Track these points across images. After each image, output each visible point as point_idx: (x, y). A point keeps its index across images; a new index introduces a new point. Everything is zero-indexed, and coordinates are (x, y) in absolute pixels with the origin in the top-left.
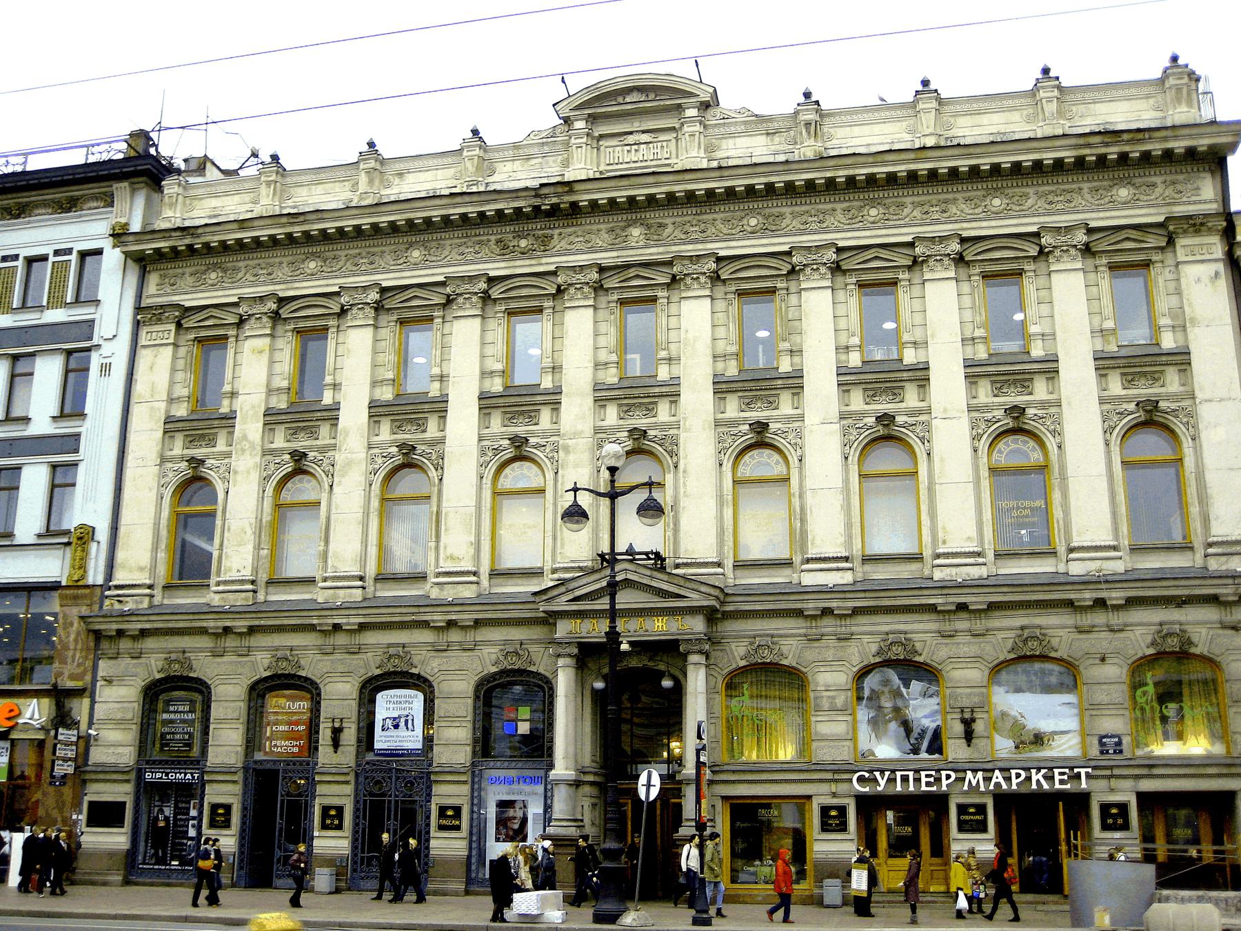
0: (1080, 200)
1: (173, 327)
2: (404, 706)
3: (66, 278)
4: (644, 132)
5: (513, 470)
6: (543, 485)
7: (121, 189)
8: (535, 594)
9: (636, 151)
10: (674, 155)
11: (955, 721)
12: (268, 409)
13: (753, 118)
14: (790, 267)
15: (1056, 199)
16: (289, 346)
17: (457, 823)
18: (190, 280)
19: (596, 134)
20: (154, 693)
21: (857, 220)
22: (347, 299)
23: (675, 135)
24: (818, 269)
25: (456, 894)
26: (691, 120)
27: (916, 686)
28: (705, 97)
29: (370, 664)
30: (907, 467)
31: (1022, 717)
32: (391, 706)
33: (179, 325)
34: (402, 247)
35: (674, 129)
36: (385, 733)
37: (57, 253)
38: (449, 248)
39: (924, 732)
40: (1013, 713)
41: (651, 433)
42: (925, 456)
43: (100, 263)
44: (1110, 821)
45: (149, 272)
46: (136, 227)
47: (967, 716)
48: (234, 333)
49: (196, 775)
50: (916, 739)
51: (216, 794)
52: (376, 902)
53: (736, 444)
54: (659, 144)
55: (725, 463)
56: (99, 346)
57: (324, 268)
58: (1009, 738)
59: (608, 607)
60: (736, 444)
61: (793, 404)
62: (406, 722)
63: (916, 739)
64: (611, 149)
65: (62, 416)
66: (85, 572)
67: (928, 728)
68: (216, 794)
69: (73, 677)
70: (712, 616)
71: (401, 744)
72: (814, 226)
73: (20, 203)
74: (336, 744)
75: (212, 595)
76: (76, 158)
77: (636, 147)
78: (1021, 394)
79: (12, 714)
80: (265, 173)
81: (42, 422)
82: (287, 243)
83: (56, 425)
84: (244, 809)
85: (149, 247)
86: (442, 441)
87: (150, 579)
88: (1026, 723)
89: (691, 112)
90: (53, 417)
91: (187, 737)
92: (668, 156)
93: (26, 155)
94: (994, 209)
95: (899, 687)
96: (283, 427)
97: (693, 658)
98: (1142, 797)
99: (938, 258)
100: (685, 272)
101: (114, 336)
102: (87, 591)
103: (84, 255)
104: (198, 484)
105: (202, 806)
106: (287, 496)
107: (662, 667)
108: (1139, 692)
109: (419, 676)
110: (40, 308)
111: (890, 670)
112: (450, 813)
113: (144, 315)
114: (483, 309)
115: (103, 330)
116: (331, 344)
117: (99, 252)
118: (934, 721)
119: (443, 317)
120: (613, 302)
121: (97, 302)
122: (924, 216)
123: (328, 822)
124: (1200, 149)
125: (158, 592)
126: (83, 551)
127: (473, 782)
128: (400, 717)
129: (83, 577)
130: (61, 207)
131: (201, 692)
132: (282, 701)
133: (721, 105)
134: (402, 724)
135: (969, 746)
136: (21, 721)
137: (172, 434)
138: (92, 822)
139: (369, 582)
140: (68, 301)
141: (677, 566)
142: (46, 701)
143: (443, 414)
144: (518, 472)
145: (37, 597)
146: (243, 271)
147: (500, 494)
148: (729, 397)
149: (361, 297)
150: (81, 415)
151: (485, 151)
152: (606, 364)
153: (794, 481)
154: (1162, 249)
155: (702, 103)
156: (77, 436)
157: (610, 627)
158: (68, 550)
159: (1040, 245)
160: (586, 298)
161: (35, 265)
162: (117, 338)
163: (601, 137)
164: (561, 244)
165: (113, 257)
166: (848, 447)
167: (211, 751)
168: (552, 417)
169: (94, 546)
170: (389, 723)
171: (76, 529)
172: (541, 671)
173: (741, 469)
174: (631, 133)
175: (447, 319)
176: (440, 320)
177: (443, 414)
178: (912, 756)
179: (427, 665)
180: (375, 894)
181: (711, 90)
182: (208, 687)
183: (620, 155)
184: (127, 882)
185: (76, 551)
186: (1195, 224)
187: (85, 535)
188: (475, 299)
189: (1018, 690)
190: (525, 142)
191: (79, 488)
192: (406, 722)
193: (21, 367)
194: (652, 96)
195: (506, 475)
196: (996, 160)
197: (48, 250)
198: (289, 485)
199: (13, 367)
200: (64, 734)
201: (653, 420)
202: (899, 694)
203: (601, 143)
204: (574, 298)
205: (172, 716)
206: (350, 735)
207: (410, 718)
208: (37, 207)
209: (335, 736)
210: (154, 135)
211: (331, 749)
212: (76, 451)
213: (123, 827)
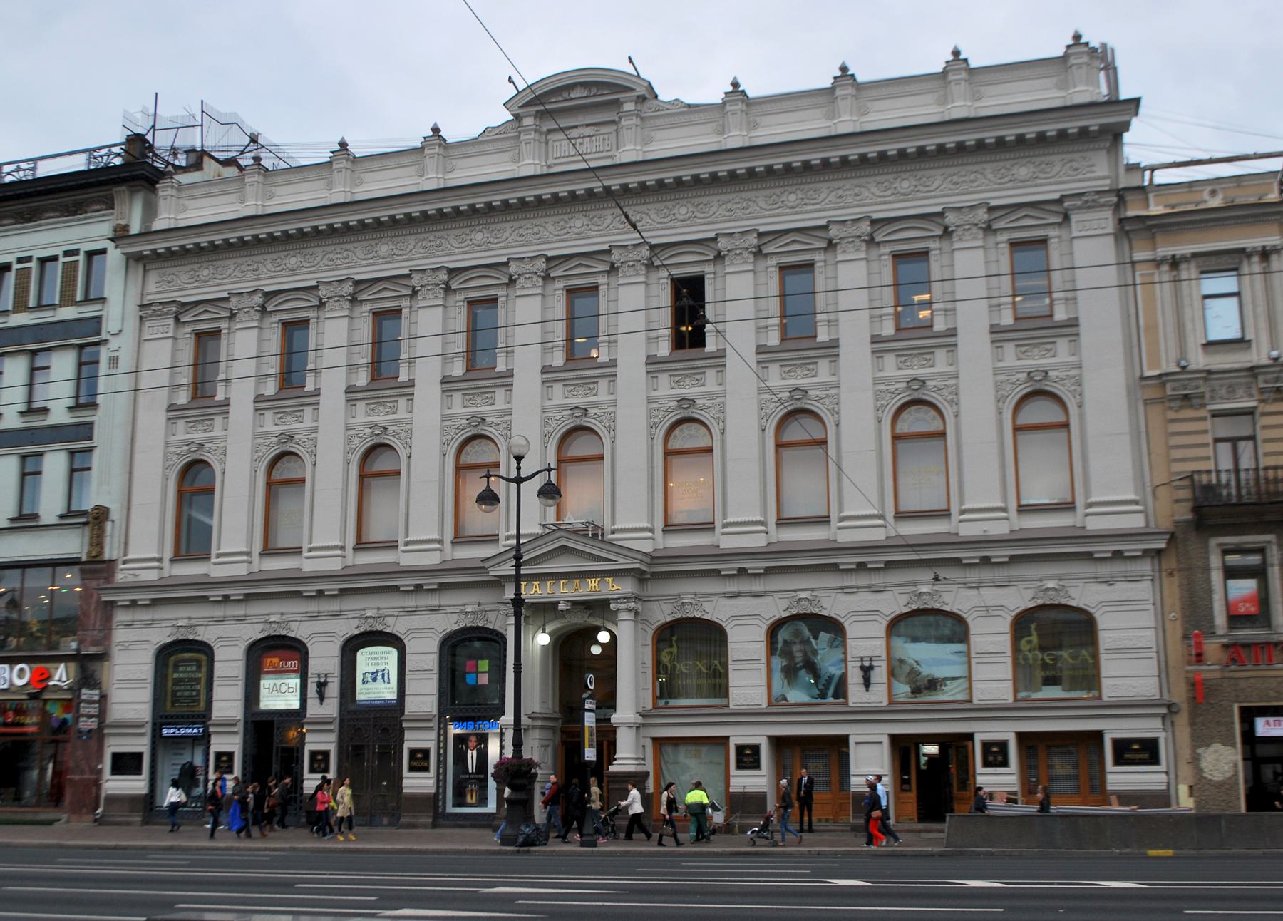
0: (867, 194)
1: (172, 322)
2: (380, 661)
3: (75, 277)
4: (587, 125)
5: (681, 430)
6: (710, 445)
7: (120, 192)
8: (484, 560)
9: (581, 144)
10: (614, 147)
11: (855, 669)
12: (349, 387)
13: (685, 109)
14: (716, 253)
15: (429, 244)
16: (188, 347)
17: (426, 764)
18: (360, 253)
19: (544, 129)
20: (166, 654)
21: (777, 206)
22: (324, 293)
23: (615, 128)
24: (633, 265)
25: (425, 826)
26: (629, 114)
27: (824, 636)
28: (640, 91)
29: (350, 628)
30: (1060, 418)
31: (918, 664)
32: (370, 662)
33: (177, 319)
34: (373, 243)
35: (613, 122)
36: (365, 686)
37: (20, 260)
38: (717, 205)
39: (831, 678)
40: (911, 661)
41: (489, 420)
42: (834, 427)
43: (104, 261)
44: (991, 758)
45: (149, 270)
46: (135, 229)
47: (867, 664)
48: (408, 304)
49: (201, 729)
50: (824, 685)
51: (218, 744)
52: (171, 834)
53: (667, 418)
54: (601, 137)
55: (1004, 411)
56: (106, 341)
57: (304, 264)
58: (907, 683)
59: (514, 573)
60: (667, 418)
61: (506, 399)
62: (383, 675)
63: (824, 685)
64: (558, 143)
65: (75, 407)
66: (102, 548)
67: (834, 675)
68: (218, 744)
69: (95, 643)
70: (641, 577)
71: (378, 695)
72: (739, 214)
73: (30, 207)
74: (867, 683)
75: (304, 560)
76: (77, 164)
77: (580, 140)
78: (923, 366)
79: (43, 677)
80: (337, 160)
81: (59, 415)
82: (284, 238)
83: (23, 420)
84: (245, 756)
85: (146, 248)
86: (510, 413)
87: (247, 547)
88: (921, 670)
89: (629, 106)
90: (69, 408)
91: (194, 693)
92: (609, 148)
93: (35, 160)
94: (903, 191)
95: (809, 638)
96: (271, 412)
97: (622, 616)
98: (1021, 736)
99: (850, 240)
100: (520, 272)
101: (120, 331)
102: (104, 565)
103: (90, 255)
104: (198, 466)
105: (208, 754)
106: (277, 475)
107: (599, 623)
108: (1023, 642)
109: (391, 635)
110: (53, 306)
111: (801, 623)
112: (419, 756)
113: (147, 310)
114: (445, 299)
115: (109, 326)
116: (224, 342)
117: (103, 252)
118: (840, 669)
119: (410, 307)
120: (559, 289)
121: (102, 300)
122: (839, 200)
123: (316, 766)
124: (988, 141)
125: (166, 563)
126: (99, 529)
127: (439, 728)
128: (377, 672)
129: (100, 553)
130: (22, 218)
131: (206, 654)
132: (275, 660)
133: (659, 98)
134: (380, 677)
135: (867, 691)
136: (52, 683)
137: (262, 412)
138: (1119, 760)
139: (349, 551)
140: (78, 299)
141: (613, 532)
142: (72, 666)
143: (509, 388)
144: (477, 448)
145: (30, 572)
146: (232, 267)
147: (366, 476)
148: (661, 376)
149: (337, 290)
150: (93, 405)
151: (445, 148)
152: (658, 338)
153: (717, 452)
154: (1059, 224)
155: (638, 97)
156: (91, 424)
157: (515, 594)
158: (87, 529)
159: (319, 296)
160: (535, 286)
161: (48, 264)
162: (122, 333)
163: (550, 131)
164: (512, 237)
165: (115, 256)
166: (764, 420)
167: (215, 705)
168: (717, 379)
169: (109, 526)
170: (369, 677)
171: (93, 509)
172: (496, 628)
173: (463, 457)
174: (576, 127)
175: (610, 287)
176: (408, 310)
177: (509, 388)
178: (819, 701)
179: (396, 626)
180: (169, 828)
181: (646, 85)
182: (304, 645)
183: (566, 148)
184: (146, 822)
185: (93, 530)
186: (1088, 201)
187: (99, 517)
188: (437, 289)
189: (915, 639)
190: (480, 139)
191: (94, 471)
192: (383, 675)
193: (40, 362)
194: (594, 91)
195: (676, 436)
196: (392, 212)
197: (58, 251)
198: (279, 465)
199: (32, 361)
200: (86, 693)
201: (301, 425)
202: (808, 642)
203: (549, 137)
204: (243, 321)
205: (182, 675)
206: (333, 690)
207: (386, 672)
208: (47, 211)
209: (321, 689)
210: (149, 138)
211: (318, 701)
212: (90, 438)
213: (140, 774)
